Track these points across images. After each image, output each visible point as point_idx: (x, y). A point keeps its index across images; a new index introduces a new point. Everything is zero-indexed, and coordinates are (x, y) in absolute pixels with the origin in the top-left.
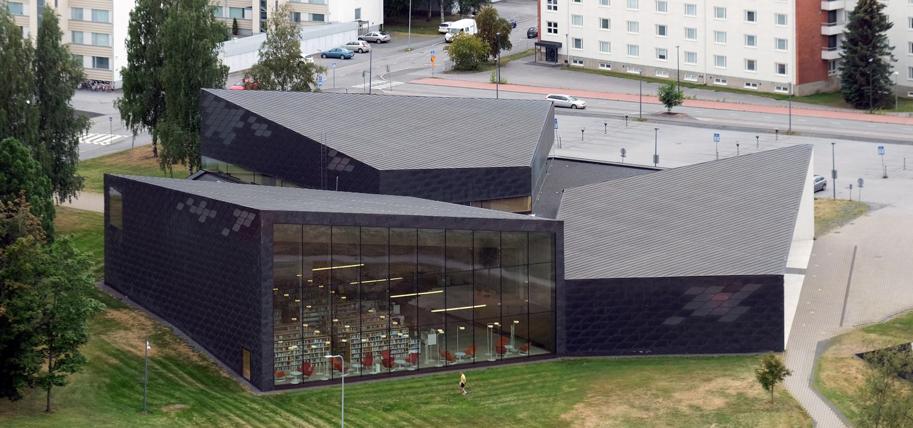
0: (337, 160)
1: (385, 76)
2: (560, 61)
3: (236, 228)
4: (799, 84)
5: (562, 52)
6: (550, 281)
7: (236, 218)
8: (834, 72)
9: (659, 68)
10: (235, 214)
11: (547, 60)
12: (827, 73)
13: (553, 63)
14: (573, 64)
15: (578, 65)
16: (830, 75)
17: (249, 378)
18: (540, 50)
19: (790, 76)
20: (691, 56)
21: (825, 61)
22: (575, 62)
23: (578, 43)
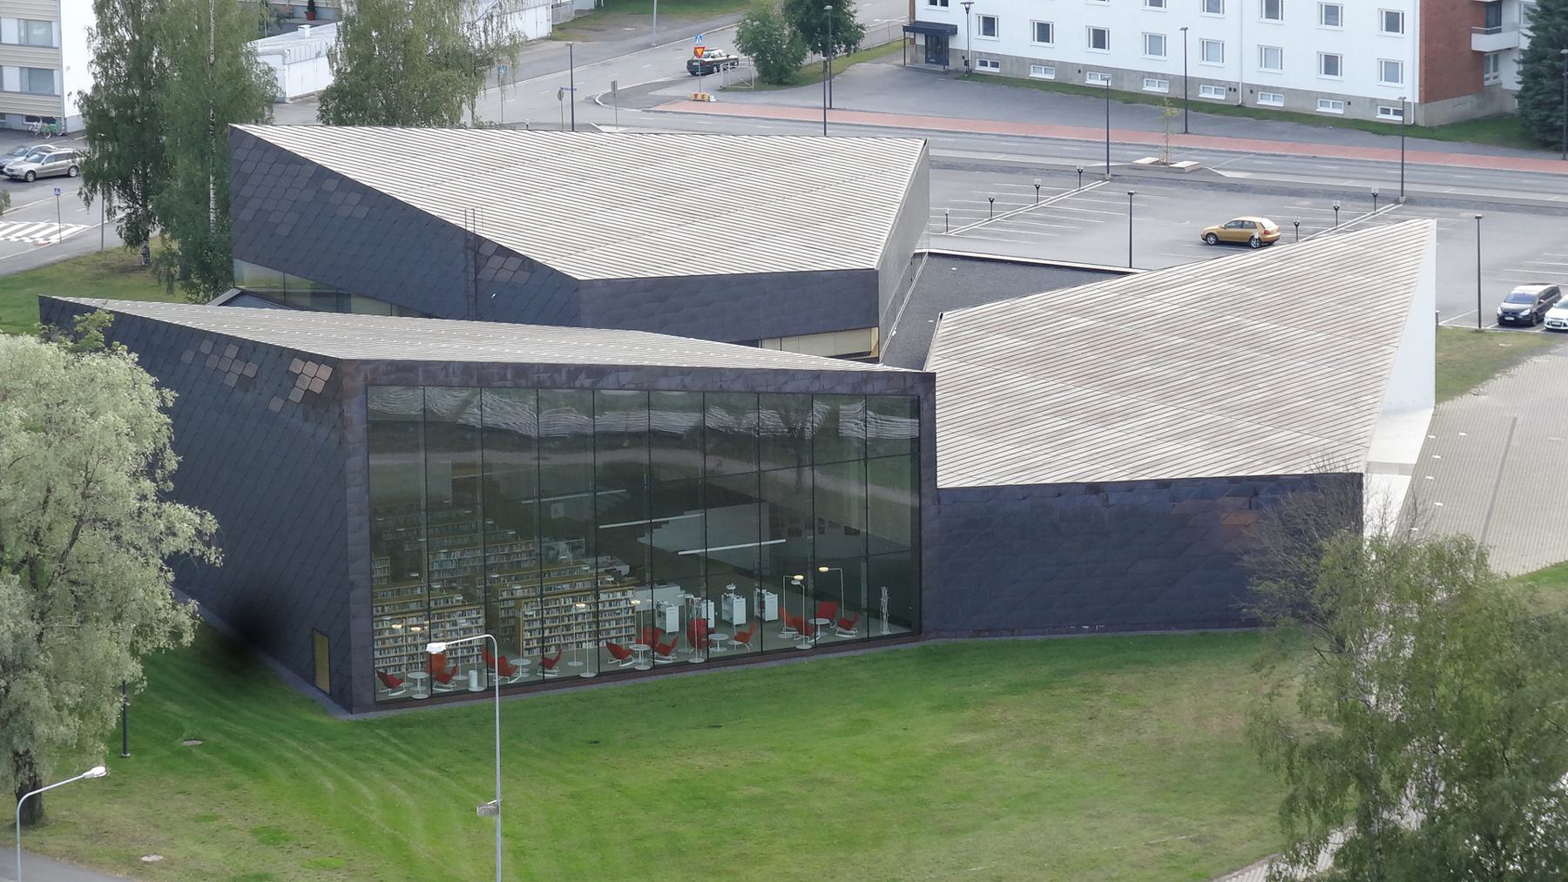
0: (498, 260)
1: (605, 98)
2: (955, 64)
3: (296, 395)
4: (1427, 101)
5: (956, 43)
6: (908, 493)
7: (296, 376)
8: (1495, 77)
9: (1264, 88)
10: (292, 368)
11: (927, 61)
12: (1482, 80)
13: (940, 68)
14: (979, 68)
15: (989, 69)
16: (1486, 83)
17: (327, 689)
18: (913, 41)
19: (1408, 88)
20: (1211, 49)
21: (1480, 55)
22: (984, 64)
23: (989, 25)
